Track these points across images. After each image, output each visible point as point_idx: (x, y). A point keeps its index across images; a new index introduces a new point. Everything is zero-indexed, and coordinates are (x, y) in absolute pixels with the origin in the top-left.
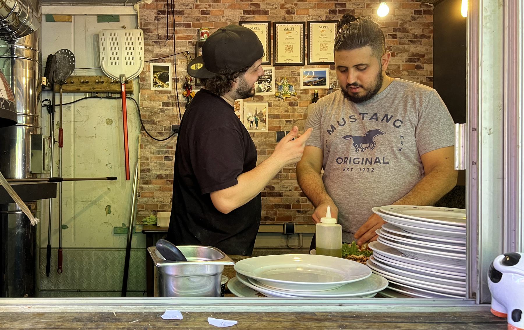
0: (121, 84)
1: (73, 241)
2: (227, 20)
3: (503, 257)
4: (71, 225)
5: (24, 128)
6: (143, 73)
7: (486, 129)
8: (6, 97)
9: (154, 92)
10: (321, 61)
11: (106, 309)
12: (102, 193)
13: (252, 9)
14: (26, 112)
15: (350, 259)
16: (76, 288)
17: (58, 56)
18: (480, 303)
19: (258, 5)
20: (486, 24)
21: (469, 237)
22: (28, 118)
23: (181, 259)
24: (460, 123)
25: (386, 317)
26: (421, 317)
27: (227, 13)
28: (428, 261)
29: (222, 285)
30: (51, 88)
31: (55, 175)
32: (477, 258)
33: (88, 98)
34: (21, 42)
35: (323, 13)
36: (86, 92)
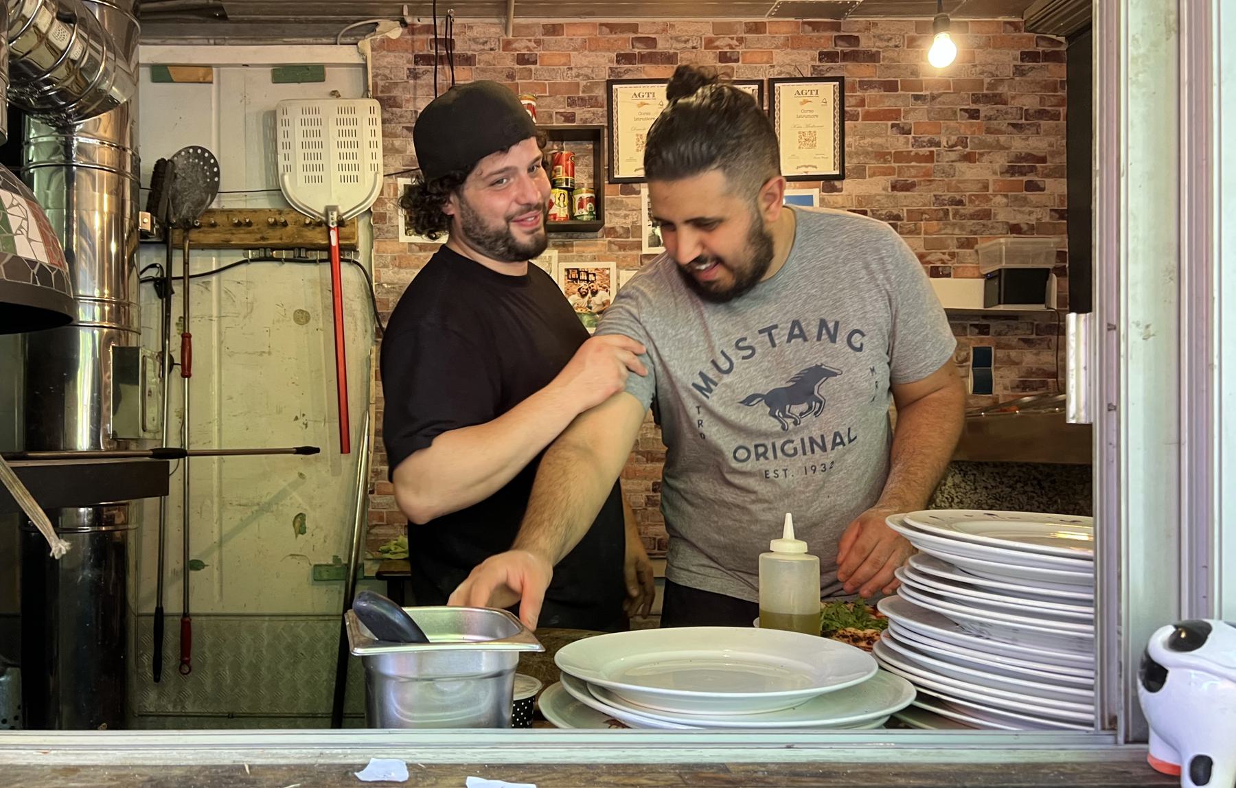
0: (329, 229)
1: (218, 598)
2: (577, 76)
3: (1169, 630)
4: (212, 561)
5: (96, 332)
6: (380, 201)
7: (1138, 325)
8: (43, 258)
9: (406, 246)
10: (801, 172)
11: (226, 758)
12: (285, 484)
13: (636, 51)
14: (102, 294)
15: (843, 637)
16: (225, 709)
17: (180, 162)
18: (1126, 742)
19: (651, 42)
20: (1137, 75)
21: (1102, 582)
22: (107, 308)
23: (414, 638)
24: (1079, 312)
25: (896, 775)
26: (981, 773)
27: (578, 59)
28: (1014, 641)
29: (518, 703)
30: (164, 238)
31: (174, 444)
32: (1119, 633)
33: (253, 260)
34: (91, 129)
35: (805, 59)
36: (246, 248)
